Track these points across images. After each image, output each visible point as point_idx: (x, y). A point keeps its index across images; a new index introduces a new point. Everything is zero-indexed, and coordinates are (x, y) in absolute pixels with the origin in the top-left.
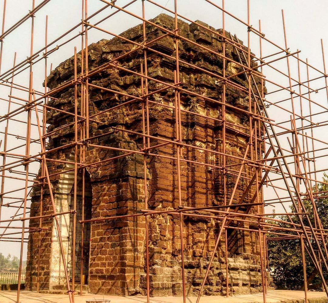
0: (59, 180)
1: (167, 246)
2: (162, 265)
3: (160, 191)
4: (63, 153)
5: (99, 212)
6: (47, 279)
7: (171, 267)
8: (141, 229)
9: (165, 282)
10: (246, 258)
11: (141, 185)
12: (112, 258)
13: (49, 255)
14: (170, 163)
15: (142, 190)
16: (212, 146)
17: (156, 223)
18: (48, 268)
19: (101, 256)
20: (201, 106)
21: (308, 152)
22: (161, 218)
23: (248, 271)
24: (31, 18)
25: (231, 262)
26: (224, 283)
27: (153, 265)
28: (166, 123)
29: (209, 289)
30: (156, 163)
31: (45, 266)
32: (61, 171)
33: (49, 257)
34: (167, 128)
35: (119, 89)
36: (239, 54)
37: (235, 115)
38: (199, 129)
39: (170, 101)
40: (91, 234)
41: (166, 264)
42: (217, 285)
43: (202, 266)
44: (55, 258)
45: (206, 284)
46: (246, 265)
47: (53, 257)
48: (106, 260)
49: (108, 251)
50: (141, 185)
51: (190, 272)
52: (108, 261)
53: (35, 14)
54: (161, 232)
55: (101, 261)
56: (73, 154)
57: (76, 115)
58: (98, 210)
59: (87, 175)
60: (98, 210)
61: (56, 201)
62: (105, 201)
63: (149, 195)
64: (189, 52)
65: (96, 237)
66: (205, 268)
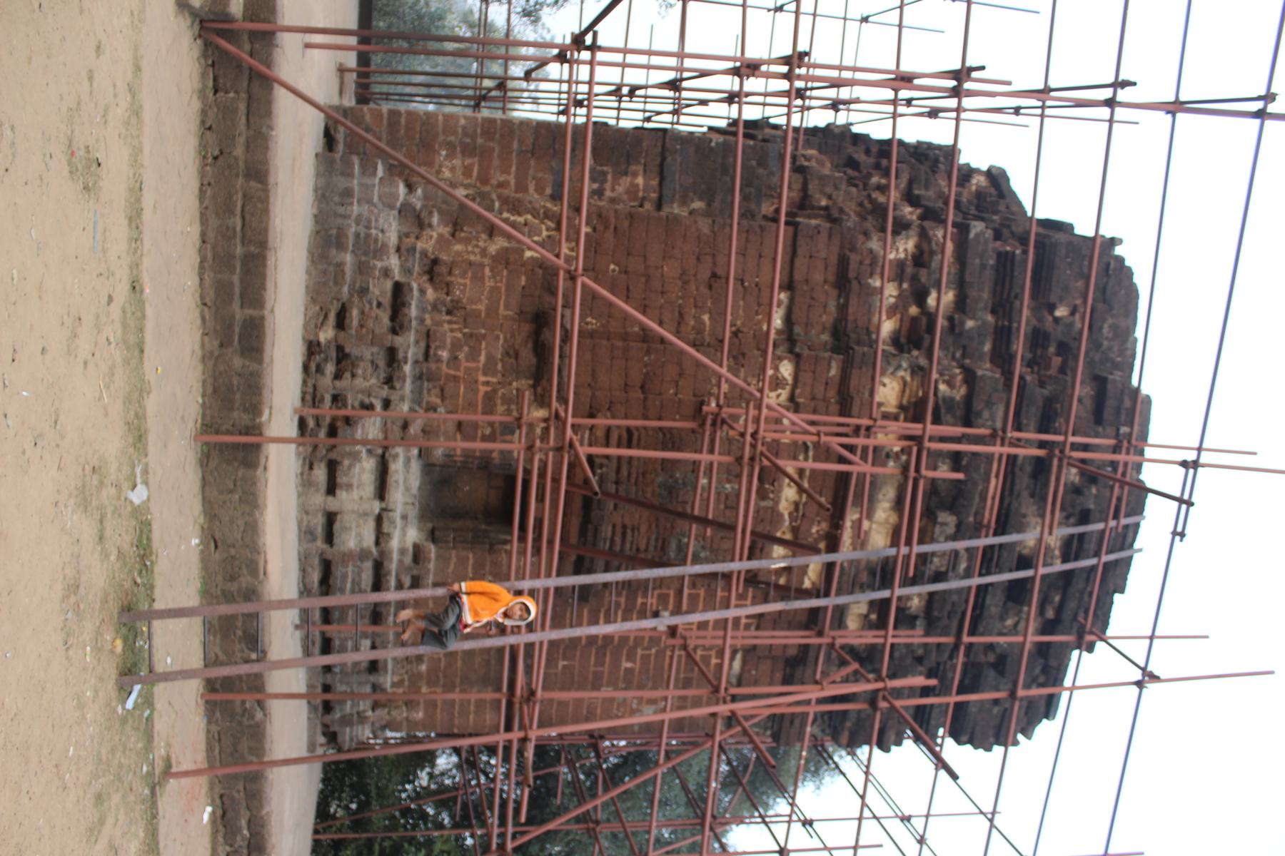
8: (512, 176)
9: (356, 209)
20: (903, 391)
25: (407, 477)
28: (834, 259)
34: (820, 265)
35: (903, 186)
38: (833, 372)
39: (900, 285)
45: (340, 349)
53: (860, 801)
64: (1058, 354)
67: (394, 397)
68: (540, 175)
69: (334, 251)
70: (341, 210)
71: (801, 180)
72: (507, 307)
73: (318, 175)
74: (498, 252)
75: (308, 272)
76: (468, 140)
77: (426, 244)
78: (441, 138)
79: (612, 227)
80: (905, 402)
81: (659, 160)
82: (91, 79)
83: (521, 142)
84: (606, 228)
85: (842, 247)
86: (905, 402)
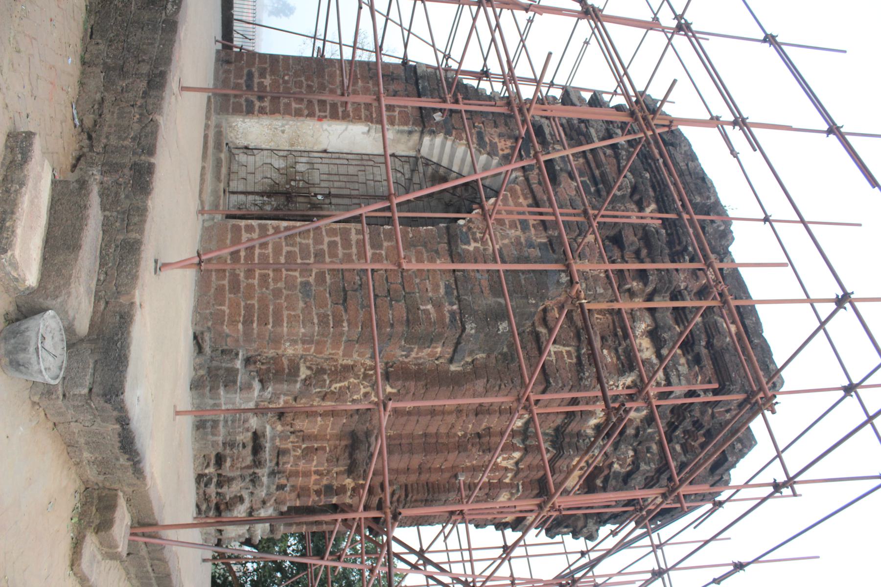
0: (452, 138)
3: (422, 391)
6: (237, 110)
13: (290, 114)
17: (352, 380)
18: (262, 111)
22: (363, 391)
24: (825, 127)
26: (222, 507)
27: (261, 381)
32: (473, 143)
42: (218, 493)
44: (283, 126)
45: (219, 475)
47: (284, 122)
50: (439, 350)
51: (244, 446)
52: (271, 275)
55: (271, 255)
58: (385, 244)
63: (415, 365)
64: (704, 435)
65: (326, 240)
69: (210, 437)
72: (332, 429)
78: (286, 338)
81: (455, 341)
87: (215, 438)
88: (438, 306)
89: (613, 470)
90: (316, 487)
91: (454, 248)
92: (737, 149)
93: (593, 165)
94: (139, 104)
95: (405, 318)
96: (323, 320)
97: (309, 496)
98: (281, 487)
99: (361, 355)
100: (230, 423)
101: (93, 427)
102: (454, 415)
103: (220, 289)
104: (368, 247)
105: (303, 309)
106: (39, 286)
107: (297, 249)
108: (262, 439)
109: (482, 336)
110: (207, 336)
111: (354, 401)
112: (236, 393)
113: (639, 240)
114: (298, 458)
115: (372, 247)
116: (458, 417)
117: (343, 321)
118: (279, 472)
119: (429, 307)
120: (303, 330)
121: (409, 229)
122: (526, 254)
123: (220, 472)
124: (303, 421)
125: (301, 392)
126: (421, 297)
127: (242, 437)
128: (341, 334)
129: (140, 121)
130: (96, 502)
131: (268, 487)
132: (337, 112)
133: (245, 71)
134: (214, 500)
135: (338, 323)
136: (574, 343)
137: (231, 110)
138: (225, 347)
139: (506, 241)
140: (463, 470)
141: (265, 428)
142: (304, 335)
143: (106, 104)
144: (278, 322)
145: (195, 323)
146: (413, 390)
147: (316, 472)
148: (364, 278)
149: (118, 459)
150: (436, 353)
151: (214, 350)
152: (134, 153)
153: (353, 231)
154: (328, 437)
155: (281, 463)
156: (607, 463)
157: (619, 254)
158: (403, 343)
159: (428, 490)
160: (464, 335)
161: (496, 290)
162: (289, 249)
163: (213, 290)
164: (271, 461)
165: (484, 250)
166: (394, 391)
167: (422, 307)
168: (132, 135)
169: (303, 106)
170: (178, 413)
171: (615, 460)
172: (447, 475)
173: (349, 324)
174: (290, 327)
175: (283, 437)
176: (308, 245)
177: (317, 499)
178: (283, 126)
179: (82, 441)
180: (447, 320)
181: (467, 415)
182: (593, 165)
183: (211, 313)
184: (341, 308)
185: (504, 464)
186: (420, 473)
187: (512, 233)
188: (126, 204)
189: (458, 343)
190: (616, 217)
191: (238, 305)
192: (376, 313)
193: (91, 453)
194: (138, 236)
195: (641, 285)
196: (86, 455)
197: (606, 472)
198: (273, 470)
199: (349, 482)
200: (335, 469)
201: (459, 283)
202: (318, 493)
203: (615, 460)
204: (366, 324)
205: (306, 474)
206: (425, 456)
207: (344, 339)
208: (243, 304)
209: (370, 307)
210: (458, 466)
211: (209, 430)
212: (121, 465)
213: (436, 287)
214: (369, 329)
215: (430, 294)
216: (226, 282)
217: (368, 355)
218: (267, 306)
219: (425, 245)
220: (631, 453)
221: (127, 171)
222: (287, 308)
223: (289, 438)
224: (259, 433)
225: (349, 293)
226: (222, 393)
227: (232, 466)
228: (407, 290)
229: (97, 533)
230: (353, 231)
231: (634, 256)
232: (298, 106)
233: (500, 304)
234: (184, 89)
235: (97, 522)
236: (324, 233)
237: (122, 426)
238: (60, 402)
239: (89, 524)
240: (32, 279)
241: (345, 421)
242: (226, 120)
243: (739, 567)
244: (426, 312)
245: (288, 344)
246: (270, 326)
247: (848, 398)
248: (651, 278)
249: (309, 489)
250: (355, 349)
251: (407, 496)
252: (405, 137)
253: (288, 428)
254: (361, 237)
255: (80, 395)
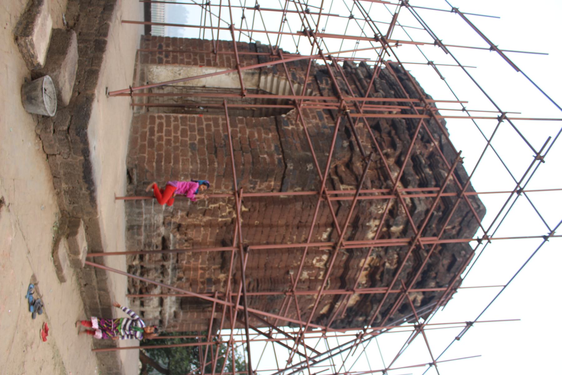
0: (277, 75)
1: (190, 218)
2: (166, 211)
3: (264, 209)
4: (312, 80)
5: (236, 127)
6: (153, 62)
7: (164, 223)
9: (144, 216)
10: (176, 314)
11: (272, 183)
12: (177, 144)
13: (184, 64)
14: (300, 222)
15: (265, 184)
16: (320, 275)
18: (168, 62)
19: (180, 129)
21: (219, 28)
22: (228, 210)
23: (159, 318)
24: (489, 47)
26: (144, 291)
29: (136, 271)
30: (301, 203)
31: (170, 59)
33: (182, 62)
36: (431, 302)
37: (357, 301)
40: (209, 116)
41: (167, 216)
43: (165, 263)
45: (142, 267)
46: (167, 315)
47: (180, 68)
48: (174, 137)
49: (186, 139)
50: (272, 183)
54: (210, 210)
56: (311, 94)
57: (366, 99)
58: (239, 125)
59: (286, 111)
60: (239, 125)
61: (250, 71)
62: (252, 134)
65: (205, 123)
66: (163, 266)
67: (165, 280)
68: (227, 183)
69: (136, 236)
70: (138, 219)
71: (350, 155)
72: (210, 238)
73: (126, 208)
74: (207, 221)
75: (126, 242)
76: (194, 173)
77: (177, 220)
78: (181, 173)
79: (257, 211)
80: (371, 264)
81: (282, 176)
82: (24, 237)
83: (218, 172)
84: (255, 210)
85: (358, 212)
86: (371, 264)
87: (139, 238)
88: (271, 155)
89: (385, 267)
90: (202, 280)
91: (279, 127)
92: (443, 76)
93: (360, 88)
94: (99, 16)
95: (251, 161)
96: (203, 162)
97: (197, 285)
98: (180, 279)
99: (226, 187)
100: (148, 227)
101: (69, 159)
102: (284, 228)
103: (143, 147)
104: (229, 127)
105: (191, 157)
106: (45, 67)
107: (188, 128)
108: (168, 242)
109: (298, 172)
110: (135, 172)
111: (222, 217)
112: (151, 205)
113: (390, 126)
114: (189, 257)
115: (231, 126)
116: (286, 230)
117: (214, 162)
118: (178, 268)
119: (266, 156)
120: (191, 167)
121: (253, 119)
122: (322, 131)
123: (142, 264)
124: (192, 231)
125: (191, 208)
126: (260, 151)
127: (156, 241)
128: (214, 170)
129: (99, 23)
130: (67, 223)
131: (172, 279)
132: (211, 63)
133: (158, 44)
134: (139, 286)
135: (212, 162)
136: (354, 183)
137: (149, 62)
138: (145, 181)
139: (310, 125)
140: (292, 268)
141: (169, 235)
142: (192, 171)
143: (81, 16)
144: (176, 161)
145: (128, 163)
146: (258, 208)
147: (202, 268)
148: (227, 141)
149: (81, 189)
150: (271, 185)
151: (139, 181)
152: (96, 36)
153: (220, 119)
154: (208, 244)
155: (179, 260)
156: (382, 263)
157: (379, 135)
158: (251, 178)
159: (271, 283)
160: (287, 171)
161: (306, 147)
162: (183, 127)
163: (138, 146)
164: (173, 258)
165: (298, 129)
166: (247, 210)
167: (261, 156)
168: (95, 28)
169: (191, 60)
170: (117, 198)
171: (386, 260)
172: (283, 272)
173: (218, 164)
174: (184, 164)
175: (180, 242)
176: (194, 126)
177: (202, 287)
178: (180, 70)
179: (62, 172)
180: (276, 163)
181: (292, 228)
182: (360, 88)
183: (137, 158)
184: (214, 156)
185: (318, 265)
186: (266, 270)
187: (314, 121)
188: (92, 55)
189: (284, 178)
190: (374, 112)
191: (153, 154)
192: (234, 158)
193: (66, 184)
194: (97, 68)
195: (392, 151)
196: (64, 186)
197: (381, 269)
198: (175, 266)
199: (222, 276)
200: (213, 267)
201: (283, 144)
202: (203, 283)
203: (386, 260)
204: (229, 164)
205: (196, 269)
206: (268, 256)
207: (216, 174)
208: (156, 153)
209: (230, 155)
210: (289, 266)
211: (136, 230)
212: (83, 194)
213: (269, 147)
214: (230, 166)
215: (266, 150)
216: (146, 143)
217: (231, 188)
218: (170, 155)
219: (263, 126)
220: (396, 256)
221: (92, 43)
222: (182, 156)
223: (184, 244)
224: (166, 238)
225: (218, 148)
226: (143, 204)
227: (150, 259)
228: (252, 148)
229: (67, 238)
230: (220, 119)
231: (387, 135)
232: (188, 60)
233: (308, 155)
234: (123, 22)
235: (68, 232)
236: (203, 120)
237: (85, 157)
238: (51, 135)
239: (63, 234)
240: (41, 59)
241: (218, 231)
242: (147, 67)
243: (469, 324)
244: (265, 159)
245: (183, 178)
246: (172, 164)
247: (520, 196)
248: (398, 145)
249: (197, 281)
250: (223, 182)
251: (258, 286)
252: (250, 77)
253: (184, 236)
254: (225, 122)
255: (63, 131)
